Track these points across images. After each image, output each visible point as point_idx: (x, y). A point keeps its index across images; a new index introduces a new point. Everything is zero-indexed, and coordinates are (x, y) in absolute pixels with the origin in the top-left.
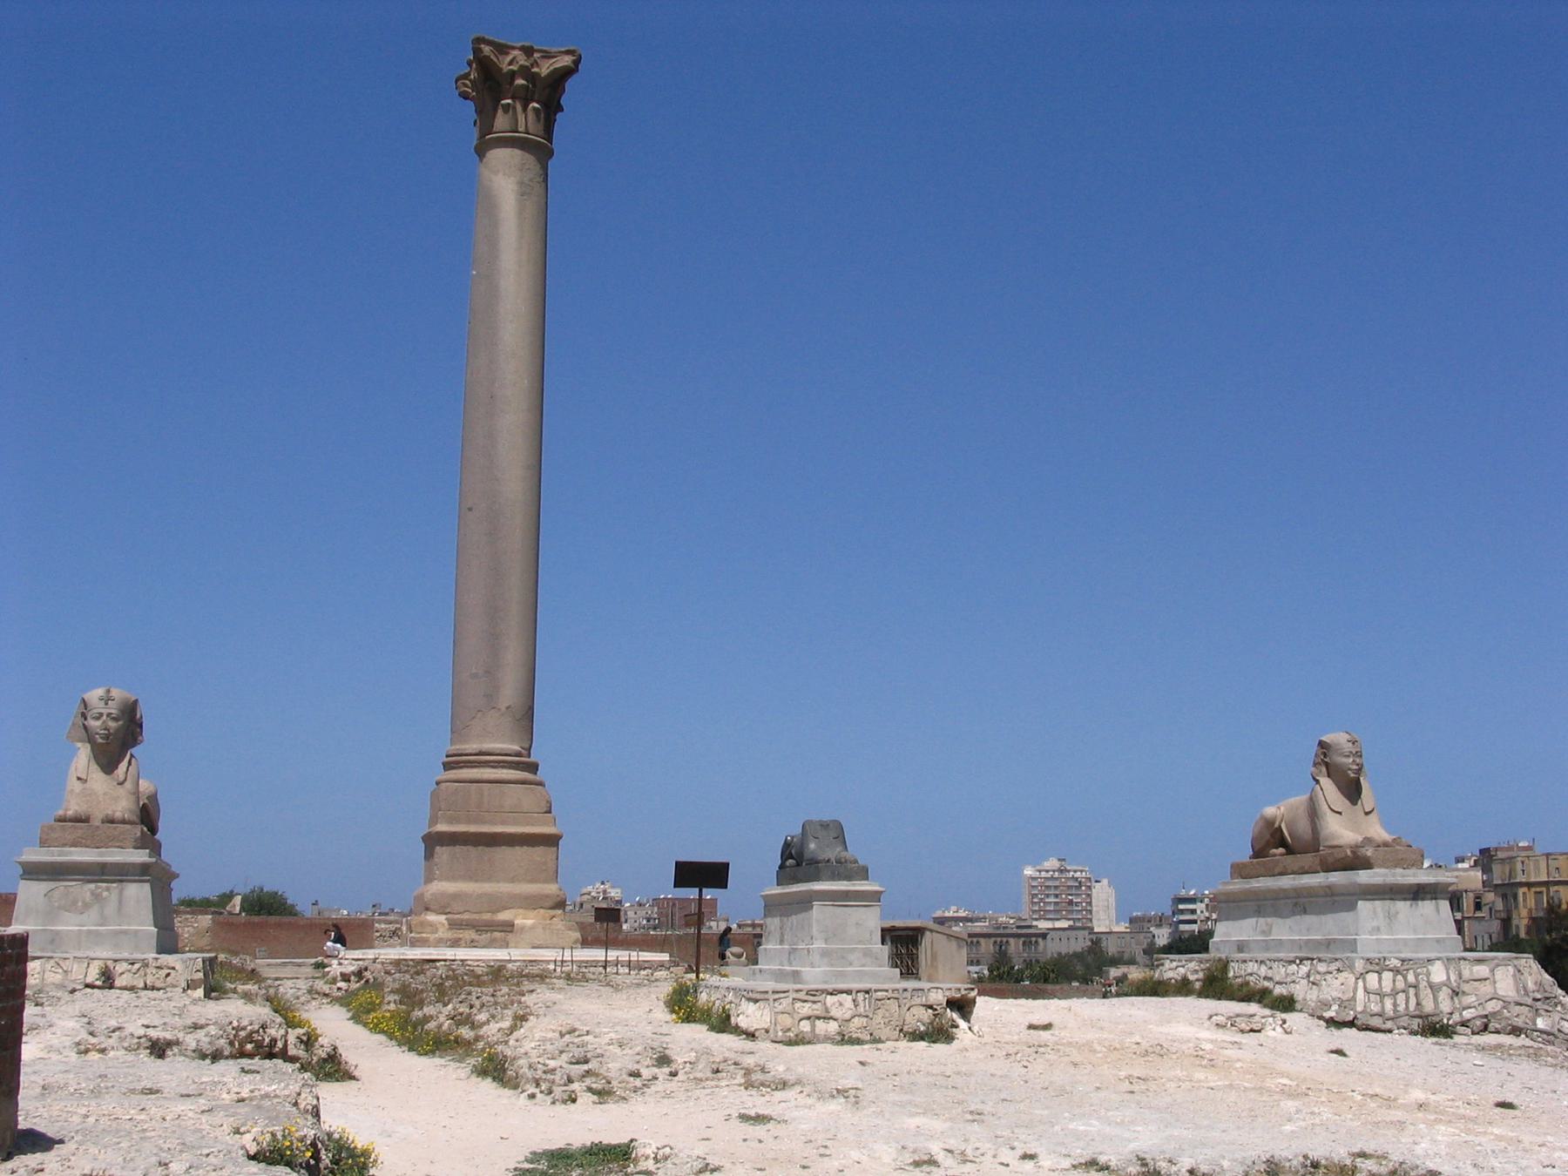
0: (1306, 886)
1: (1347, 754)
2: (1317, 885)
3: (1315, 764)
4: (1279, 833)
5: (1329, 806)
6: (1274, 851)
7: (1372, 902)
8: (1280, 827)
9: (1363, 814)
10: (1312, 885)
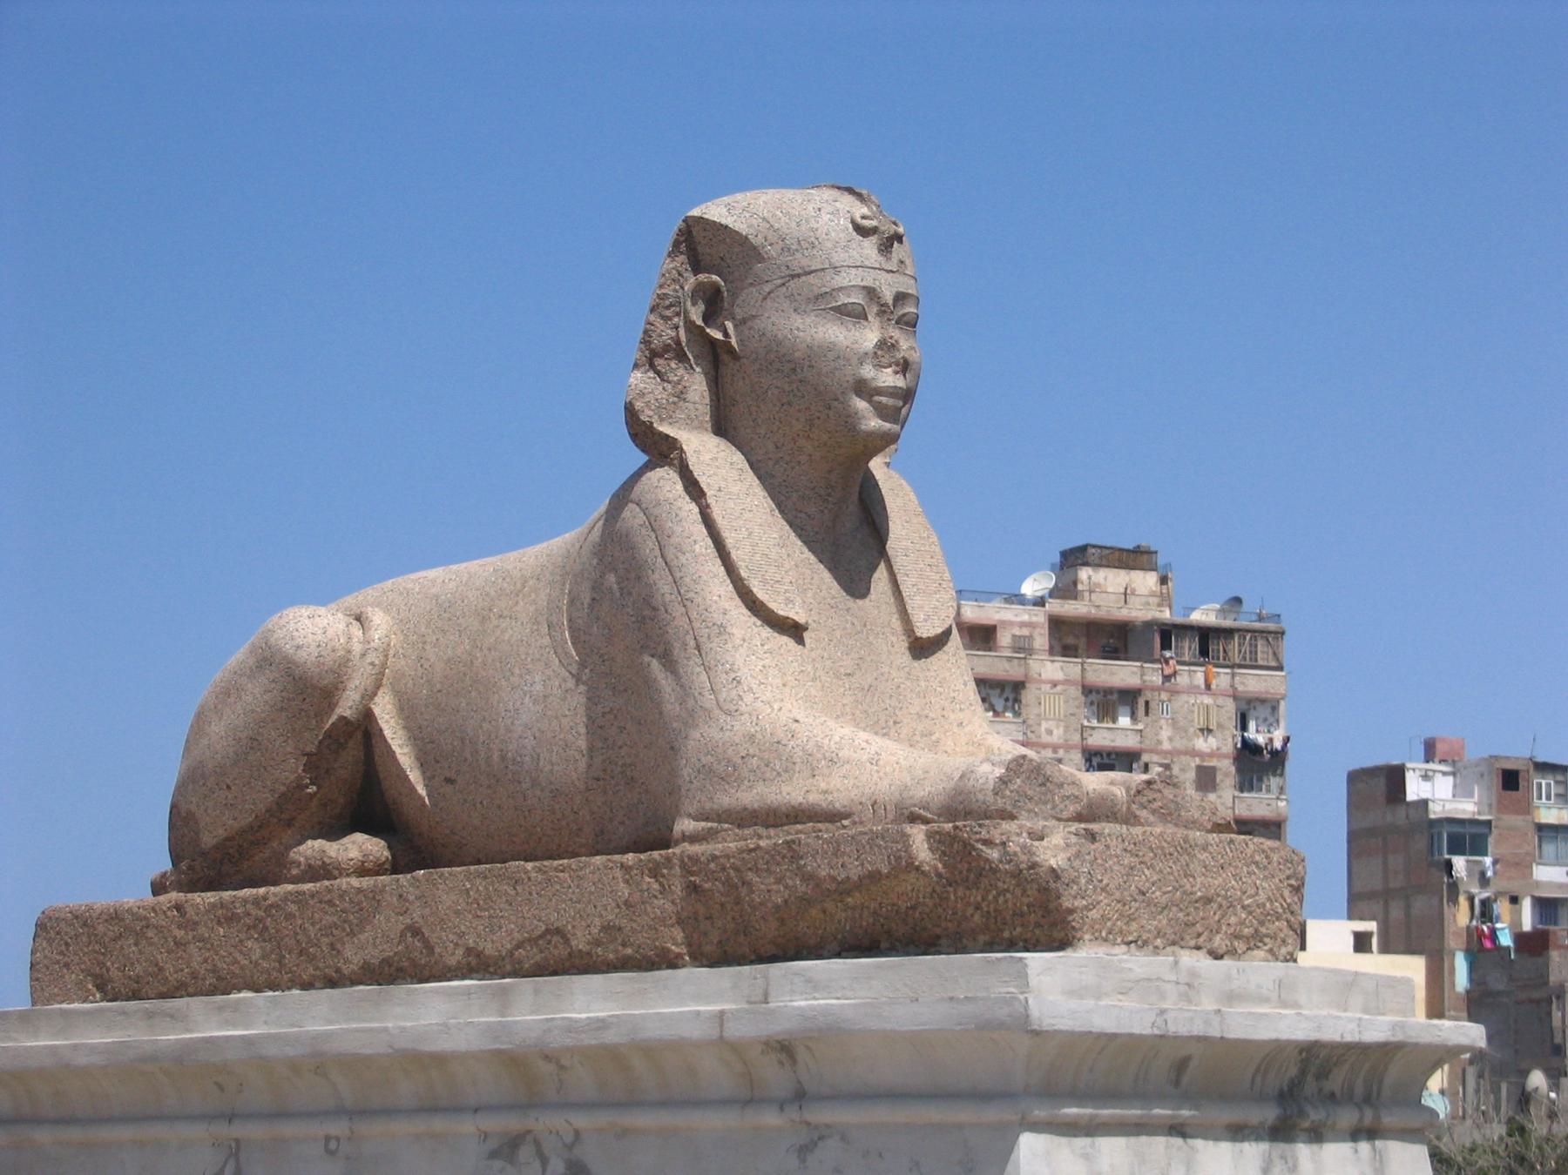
0: (611, 1037)
1: (857, 298)
2: (695, 1032)
3: (652, 357)
4: (352, 753)
5: (754, 606)
6: (314, 847)
7: (1081, 1142)
8: (368, 716)
9: (902, 644)
10: (653, 1032)
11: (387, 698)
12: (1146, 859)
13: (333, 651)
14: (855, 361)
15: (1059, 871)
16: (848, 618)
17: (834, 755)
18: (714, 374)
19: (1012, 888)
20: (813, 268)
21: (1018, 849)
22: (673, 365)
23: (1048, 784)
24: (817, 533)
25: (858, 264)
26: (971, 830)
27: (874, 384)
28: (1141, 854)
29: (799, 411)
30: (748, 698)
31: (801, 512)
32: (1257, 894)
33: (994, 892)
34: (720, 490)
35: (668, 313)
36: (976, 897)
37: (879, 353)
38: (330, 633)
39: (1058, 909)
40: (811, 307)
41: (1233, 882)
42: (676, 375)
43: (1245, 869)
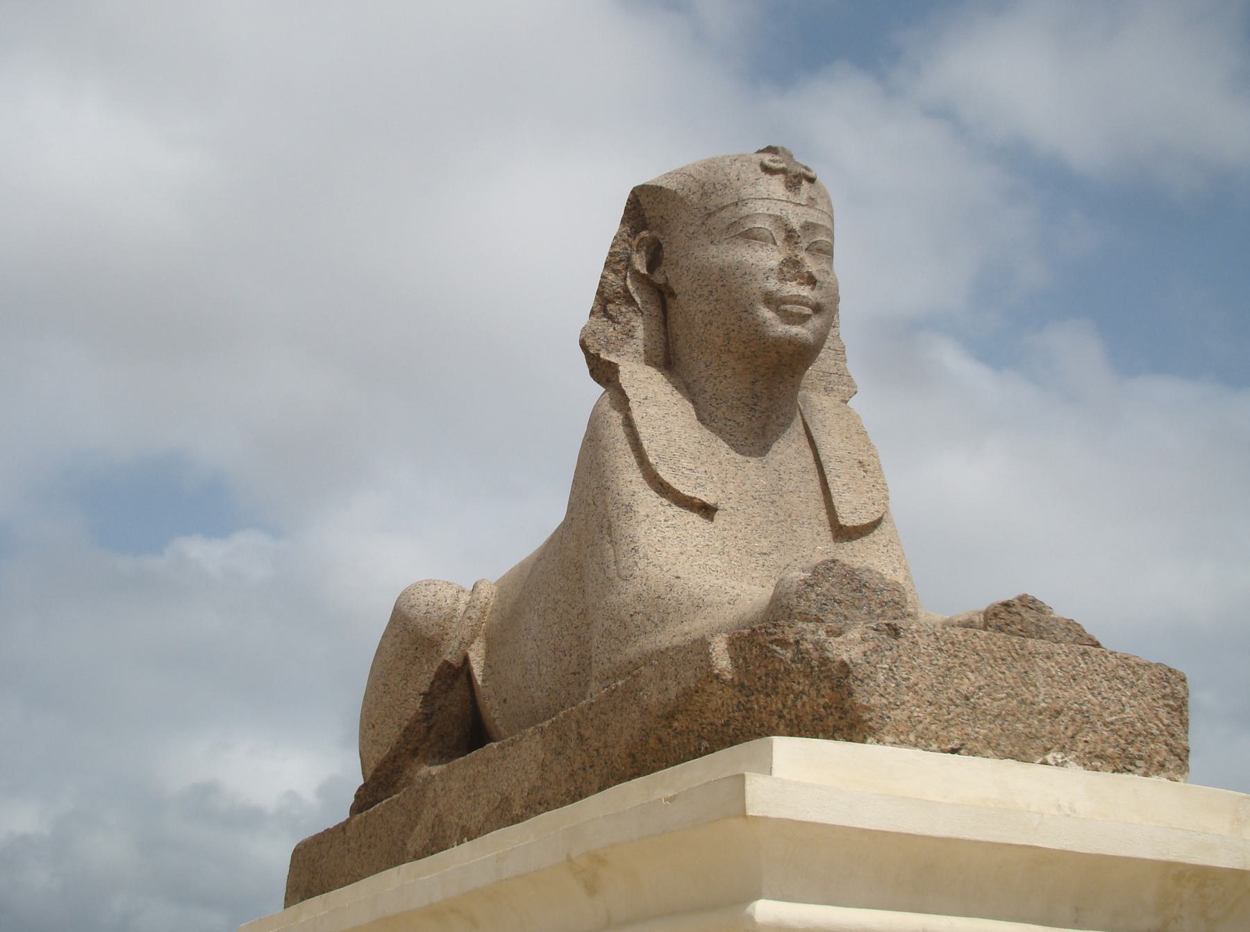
5: (663, 489)
11: (482, 644)
12: (968, 661)
13: (440, 609)
14: (760, 276)
15: (851, 666)
16: (772, 508)
17: (701, 601)
18: (661, 315)
19: (807, 689)
20: (725, 204)
21: (811, 646)
22: (623, 310)
25: (766, 197)
26: (766, 632)
27: (779, 295)
28: (961, 655)
29: (718, 328)
30: (642, 564)
31: (730, 420)
32: (1123, 711)
33: (792, 696)
34: (646, 399)
35: (619, 267)
36: (776, 703)
37: (785, 269)
38: (440, 595)
39: (854, 707)
40: (724, 237)
41: (1090, 696)
42: (625, 317)
43: (1105, 683)
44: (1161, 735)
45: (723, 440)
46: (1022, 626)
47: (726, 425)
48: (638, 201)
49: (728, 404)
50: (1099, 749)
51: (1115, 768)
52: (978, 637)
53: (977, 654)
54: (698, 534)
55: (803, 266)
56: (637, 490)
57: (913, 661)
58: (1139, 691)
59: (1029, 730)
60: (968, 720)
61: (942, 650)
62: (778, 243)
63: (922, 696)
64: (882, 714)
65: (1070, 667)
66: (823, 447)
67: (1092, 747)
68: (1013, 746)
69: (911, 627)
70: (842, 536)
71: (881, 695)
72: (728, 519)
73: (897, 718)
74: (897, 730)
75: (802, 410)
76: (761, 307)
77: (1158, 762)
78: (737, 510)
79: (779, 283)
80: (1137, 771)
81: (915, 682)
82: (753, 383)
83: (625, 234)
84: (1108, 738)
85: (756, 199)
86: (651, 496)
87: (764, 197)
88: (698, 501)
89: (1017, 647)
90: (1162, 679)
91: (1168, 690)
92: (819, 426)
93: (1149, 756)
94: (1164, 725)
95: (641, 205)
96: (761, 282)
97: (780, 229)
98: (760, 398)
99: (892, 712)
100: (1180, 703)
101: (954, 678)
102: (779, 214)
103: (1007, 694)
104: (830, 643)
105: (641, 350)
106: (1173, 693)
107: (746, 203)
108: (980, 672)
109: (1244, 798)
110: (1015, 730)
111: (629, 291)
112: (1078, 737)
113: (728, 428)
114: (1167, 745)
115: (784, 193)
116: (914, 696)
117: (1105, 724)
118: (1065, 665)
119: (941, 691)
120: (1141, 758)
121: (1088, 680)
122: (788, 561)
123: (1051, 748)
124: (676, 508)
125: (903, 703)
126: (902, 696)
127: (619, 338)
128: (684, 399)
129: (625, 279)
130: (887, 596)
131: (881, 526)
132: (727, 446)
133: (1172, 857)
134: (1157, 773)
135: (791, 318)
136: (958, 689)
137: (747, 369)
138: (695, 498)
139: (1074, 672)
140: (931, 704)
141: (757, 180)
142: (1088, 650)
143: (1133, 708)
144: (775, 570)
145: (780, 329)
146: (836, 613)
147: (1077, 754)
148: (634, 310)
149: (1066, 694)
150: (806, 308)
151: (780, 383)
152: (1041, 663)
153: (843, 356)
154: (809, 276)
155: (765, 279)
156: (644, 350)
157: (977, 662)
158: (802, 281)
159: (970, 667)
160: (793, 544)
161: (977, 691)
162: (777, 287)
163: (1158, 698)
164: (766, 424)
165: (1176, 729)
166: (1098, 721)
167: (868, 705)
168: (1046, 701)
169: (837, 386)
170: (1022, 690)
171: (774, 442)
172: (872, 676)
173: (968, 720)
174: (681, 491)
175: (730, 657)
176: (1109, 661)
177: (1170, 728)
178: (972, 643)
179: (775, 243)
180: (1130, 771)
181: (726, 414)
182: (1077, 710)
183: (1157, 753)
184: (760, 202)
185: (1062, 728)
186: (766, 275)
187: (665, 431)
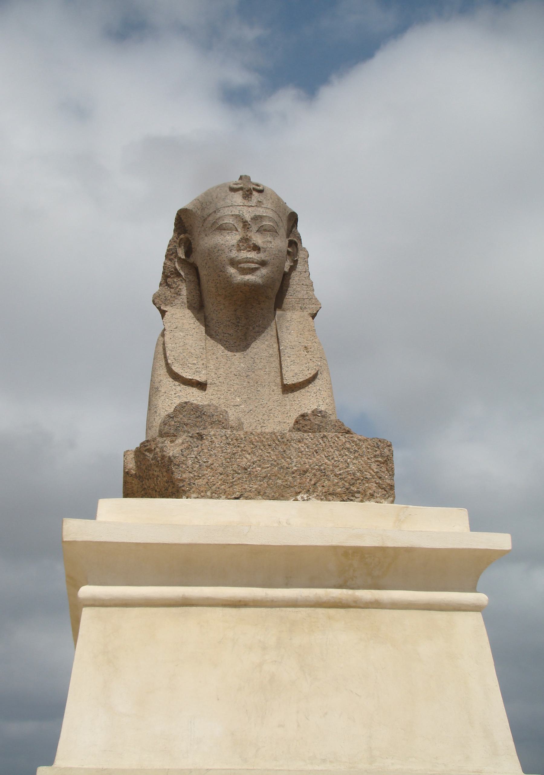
5: (176, 377)
15: (172, 458)
20: (210, 212)
22: (175, 280)
23: (203, 416)
24: (235, 342)
25: (230, 205)
27: (237, 259)
31: (226, 333)
34: (176, 328)
35: (172, 257)
37: (241, 244)
41: (327, 461)
43: (337, 453)
44: (373, 478)
45: (221, 345)
46: (311, 427)
47: (224, 336)
48: (181, 218)
49: (224, 324)
50: (331, 490)
51: (342, 499)
52: (253, 435)
53: (252, 444)
54: (194, 399)
55: (250, 241)
56: (162, 379)
57: (211, 452)
58: (359, 455)
59: (286, 483)
60: (246, 481)
61: (230, 444)
62: (239, 230)
63: (216, 470)
64: (190, 482)
65: (314, 446)
66: (283, 341)
67: (327, 489)
68: (275, 493)
69: (210, 433)
70: (287, 390)
71: (190, 472)
72: (216, 388)
73: (199, 484)
74: (200, 490)
75: (276, 321)
76: (229, 267)
77: (370, 494)
78: (223, 383)
79: (237, 253)
80: (357, 500)
81: (211, 463)
82: (235, 311)
83: (175, 238)
84: (338, 483)
85: (224, 207)
86: (169, 381)
87: (229, 205)
88: (195, 381)
89: (279, 437)
90: (375, 446)
91: (378, 452)
92: (284, 330)
93: (364, 491)
94: (374, 473)
95: (182, 221)
96: (227, 253)
97: (240, 222)
98: (240, 319)
99: (196, 481)
100: (386, 459)
101: (237, 459)
102: (238, 213)
103: (271, 464)
104: (167, 447)
105: (185, 301)
106: (381, 454)
107: (220, 211)
108: (254, 454)
109: (404, 507)
110: (276, 483)
111: (177, 270)
112: (318, 484)
113: (225, 338)
114: (376, 483)
115: (242, 201)
116: (211, 471)
117: (336, 475)
118: (311, 445)
119: (228, 466)
120: (359, 492)
121: (325, 451)
122: (251, 408)
123: (301, 492)
124: (182, 386)
125: (204, 475)
126: (203, 472)
127: (173, 296)
128: (201, 325)
129: (174, 264)
130: (215, 418)
131: (314, 382)
132: (223, 348)
133: (335, 543)
134: (369, 499)
135: (245, 271)
136: (239, 464)
137: (231, 303)
138: (193, 379)
139: (317, 448)
140: (221, 474)
141: (226, 196)
142: (326, 435)
143: (355, 465)
144: (242, 414)
145: (239, 278)
146: (184, 431)
147: (317, 493)
148: (181, 280)
149: (310, 461)
150: (252, 264)
151: (251, 308)
152: (294, 445)
153: (312, 288)
154: (254, 246)
155: (230, 252)
156: (187, 301)
157: (252, 448)
158: (249, 249)
159: (248, 451)
160: (256, 398)
161: (252, 464)
162: (236, 255)
163: (371, 458)
164: (246, 333)
165: (382, 474)
166: (332, 474)
167: (182, 478)
168: (297, 466)
169: (308, 306)
170: (281, 461)
171: (253, 342)
172: (184, 462)
173: (246, 481)
174: (185, 376)
175: (135, 462)
176: (340, 440)
177: (378, 474)
178: (249, 438)
179: (237, 230)
180: (352, 500)
181: (224, 330)
182: (318, 469)
183: (370, 488)
184: (227, 209)
185: (308, 480)
186: (230, 249)
187: (183, 344)
